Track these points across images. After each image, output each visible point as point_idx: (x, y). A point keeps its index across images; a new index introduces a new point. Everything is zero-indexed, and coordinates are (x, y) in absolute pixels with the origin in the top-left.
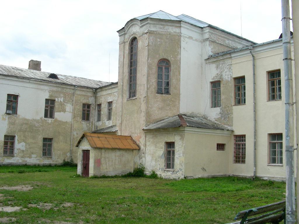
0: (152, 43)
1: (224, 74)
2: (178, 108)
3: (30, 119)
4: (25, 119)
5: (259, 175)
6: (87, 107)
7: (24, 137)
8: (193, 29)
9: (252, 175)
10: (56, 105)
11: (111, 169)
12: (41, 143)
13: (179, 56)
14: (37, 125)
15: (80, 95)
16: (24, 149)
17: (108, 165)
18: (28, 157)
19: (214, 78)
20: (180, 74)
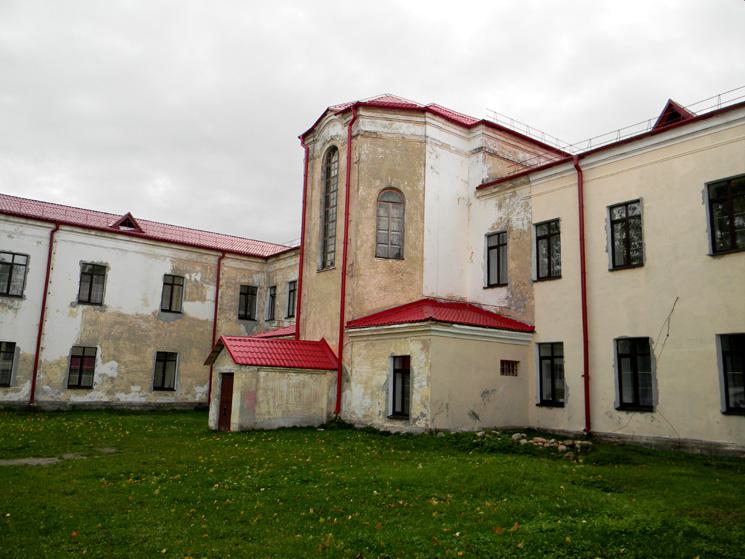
0: (367, 156)
1: (514, 218)
2: (420, 287)
3: (130, 313)
4: (120, 315)
5: (40, 397)
6: (248, 293)
7: (115, 349)
8: (452, 130)
10: (187, 288)
11: (279, 413)
12: (151, 363)
13: (421, 184)
14: (144, 325)
15: (235, 269)
16: (115, 375)
17: (271, 404)
18: (122, 391)
19: (493, 227)
20: (423, 219)
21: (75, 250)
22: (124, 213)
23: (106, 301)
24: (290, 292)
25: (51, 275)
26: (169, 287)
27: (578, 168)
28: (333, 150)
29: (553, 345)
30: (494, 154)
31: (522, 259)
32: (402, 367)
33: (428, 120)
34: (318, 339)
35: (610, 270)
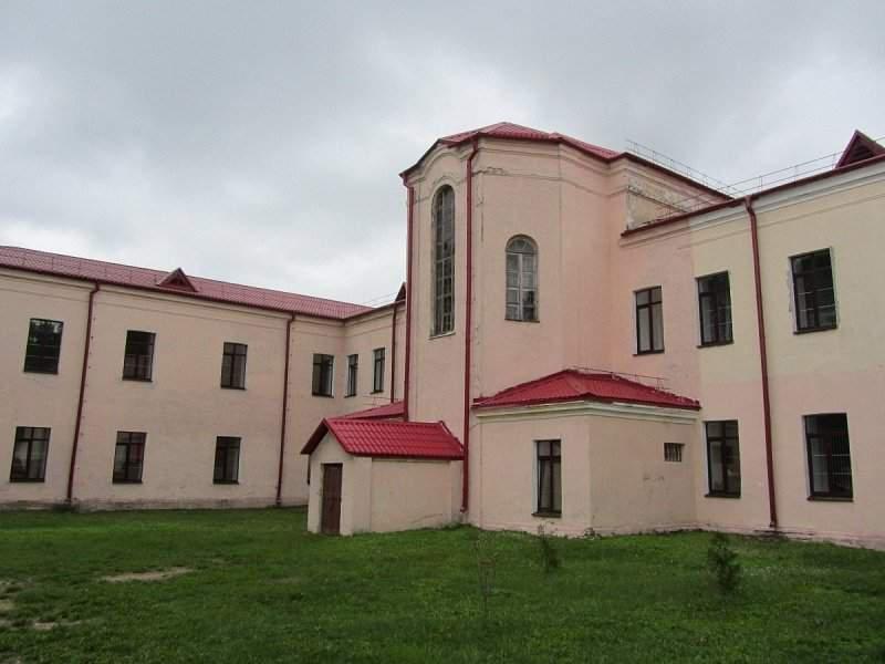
6: (323, 365)
9: (764, 524)
21: (119, 316)
22: (170, 268)
23: (246, 387)
24: (376, 361)
25: (290, 362)
26: (230, 357)
27: (751, 211)
28: (446, 191)
29: (723, 424)
30: (638, 194)
31: (682, 314)
32: (549, 456)
33: (562, 153)
34: (433, 420)
35: (795, 333)
